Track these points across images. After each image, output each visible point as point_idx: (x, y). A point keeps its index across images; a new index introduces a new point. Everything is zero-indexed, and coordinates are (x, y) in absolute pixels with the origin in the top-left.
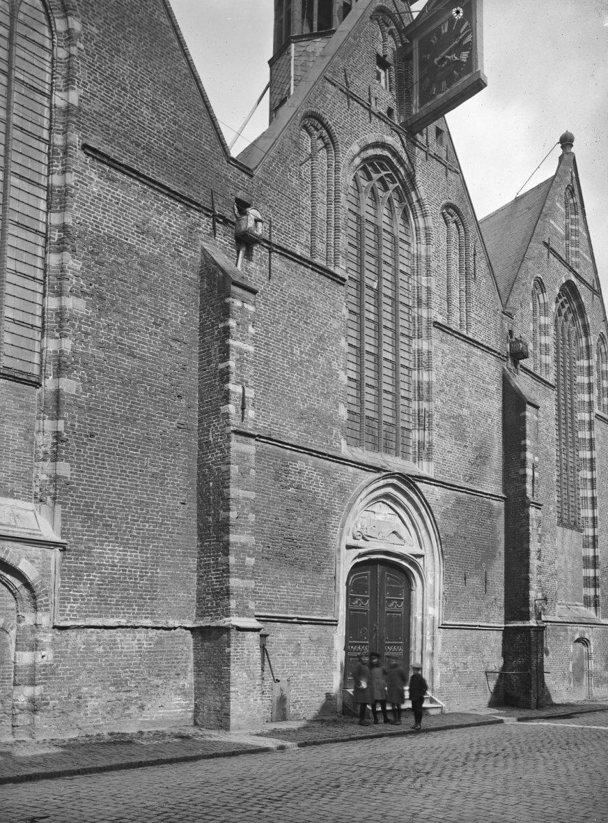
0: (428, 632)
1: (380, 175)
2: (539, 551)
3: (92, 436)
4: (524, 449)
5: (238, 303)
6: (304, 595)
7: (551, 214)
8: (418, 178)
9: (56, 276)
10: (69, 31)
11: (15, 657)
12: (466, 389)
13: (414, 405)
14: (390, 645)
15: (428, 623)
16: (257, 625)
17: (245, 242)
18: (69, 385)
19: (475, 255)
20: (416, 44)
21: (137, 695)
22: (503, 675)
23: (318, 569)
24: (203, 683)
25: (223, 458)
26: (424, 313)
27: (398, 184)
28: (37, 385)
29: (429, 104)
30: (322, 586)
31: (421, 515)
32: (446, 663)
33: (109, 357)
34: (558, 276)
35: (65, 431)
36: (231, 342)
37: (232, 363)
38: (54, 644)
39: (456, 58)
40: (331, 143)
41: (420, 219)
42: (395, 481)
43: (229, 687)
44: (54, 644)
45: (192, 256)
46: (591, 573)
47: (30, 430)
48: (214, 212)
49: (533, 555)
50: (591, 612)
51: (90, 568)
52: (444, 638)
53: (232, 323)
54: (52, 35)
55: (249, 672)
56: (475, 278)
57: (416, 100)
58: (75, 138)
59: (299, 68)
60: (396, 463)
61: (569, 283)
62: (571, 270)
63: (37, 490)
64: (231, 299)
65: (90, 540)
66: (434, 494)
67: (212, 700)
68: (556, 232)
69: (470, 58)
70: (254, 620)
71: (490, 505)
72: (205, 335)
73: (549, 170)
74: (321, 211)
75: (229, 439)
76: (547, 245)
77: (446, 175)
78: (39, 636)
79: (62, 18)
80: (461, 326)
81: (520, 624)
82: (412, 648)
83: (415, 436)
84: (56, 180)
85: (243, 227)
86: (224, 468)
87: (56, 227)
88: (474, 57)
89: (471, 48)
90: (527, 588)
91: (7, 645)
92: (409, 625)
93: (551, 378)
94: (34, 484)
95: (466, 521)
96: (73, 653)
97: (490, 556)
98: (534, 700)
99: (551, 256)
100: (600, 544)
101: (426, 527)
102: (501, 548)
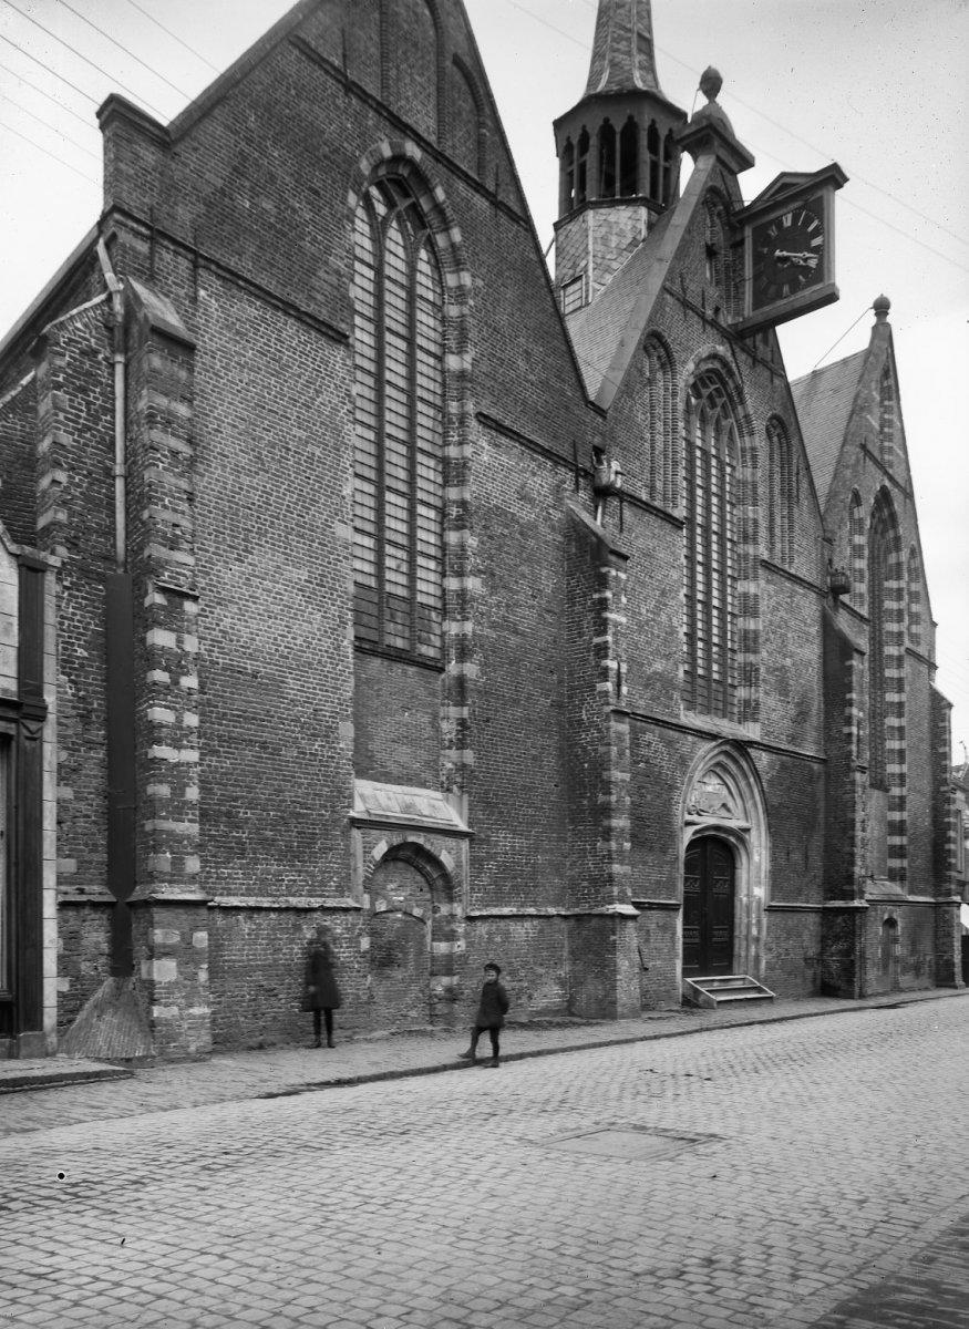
2: (863, 822)
3: (488, 721)
5: (613, 573)
6: (654, 878)
11: (431, 949)
12: (789, 635)
13: (740, 657)
14: (719, 929)
17: (602, 493)
18: (471, 669)
19: (798, 474)
20: (748, 232)
21: (526, 984)
23: (664, 850)
27: (725, 399)
31: (749, 785)
32: (770, 950)
34: (872, 482)
35: (470, 718)
36: (611, 616)
38: (467, 935)
42: (727, 748)
44: (467, 935)
46: (897, 840)
47: (435, 716)
51: (492, 857)
54: (443, 291)
55: (630, 960)
58: (470, 407)
60: (727, 727)
61: (883, 488)
65: (489, 829)
68: (872, 427)
69: (820, 265)
70: (631, 907)
71: (811, 769)
77: (772, 381)
78: (454, 926)
79: (453, 272)
84: (453, 452)
86: (602, 749)
87: (454, 502)
88: (825, 265)
89: (824, 253)
90: (853, 864)
92: (732, 907)
93: (864, 612)
94: (441, 773)
98: (857, 990)
100: (908, 806)
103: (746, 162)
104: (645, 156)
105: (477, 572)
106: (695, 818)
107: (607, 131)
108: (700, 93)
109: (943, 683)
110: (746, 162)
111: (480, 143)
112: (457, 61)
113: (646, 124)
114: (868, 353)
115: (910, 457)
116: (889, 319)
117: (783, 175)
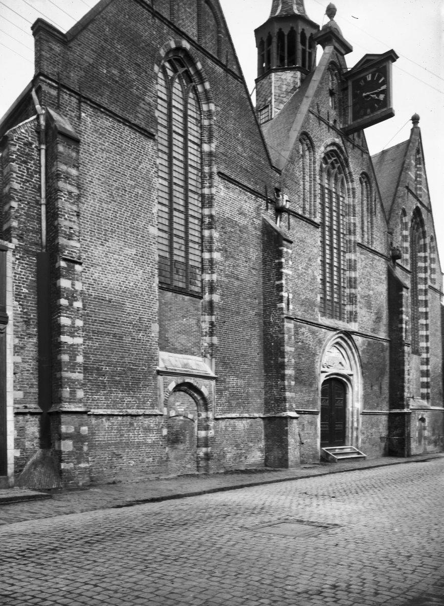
0: (355, 417)
1: (332, 160)
4: (402, 313)
6: (306, 399)
7: (408, 169)
8: (350, 160)
9: (208, 241)
10: (209, 111)
12: (372, 280)
13: (347, 291)
15: (355, 412)
16: (297, 415)
20: (350, 83)
22: (389, 438)
24: (270, 445)
25: (280, 331)
26: (352, 238)
28: (201, 298)
29: (359, 120)
30: (312, 394)
31: (352, 353)
32: (363, 433)
33: (230, 281)
36: (283, 270)
37: (283, 282)
38: (215, 427)
39: (376, 98)
40: (312, 147)
41: (350, 184)
43: (287, 447)
45: (258, 222)
47: (199, 321)
48: (266, 198)
49: (406, 373)
50: (425, 403)
52: (363, 420)
53: (283, 260)
56: (375, 215)
57: (350, 116)
58: (215, 169)
59: (277, 88)
60: (342, 325)
61: (417, 208)
62: (418, 200)
63: (203, 351)
64: (282, 248)
66: (359, 340)
67: (277, 453)
71: (383, 345)
72: (266, 265)
73: (407, 137)
74: (307, 185)
75: (283, 321)
76: (407, 187)
78: (209, 423)
79: (206, 104)
80: (368, 243)
81: (398, 411)
82: (347, 425)
83: (348, 308)
84: (206, 191)
85: (281, 205)
86: (280, 336)
87: (207, 216)
89: (387, 92)
91: (193, 428)
95: (372, 354)
96: (221, 431)
97: (382, 374)
98: (406, 453)
99: (409, 194)
100: (430, 363)
101: (354, 359)
102: (388, 369)
103: (349, 50)
104: (300, 47)
105: (219, 250)
107: (281, 34)
110: (349, 50)
113: (300, 31)
116: (419, 125)
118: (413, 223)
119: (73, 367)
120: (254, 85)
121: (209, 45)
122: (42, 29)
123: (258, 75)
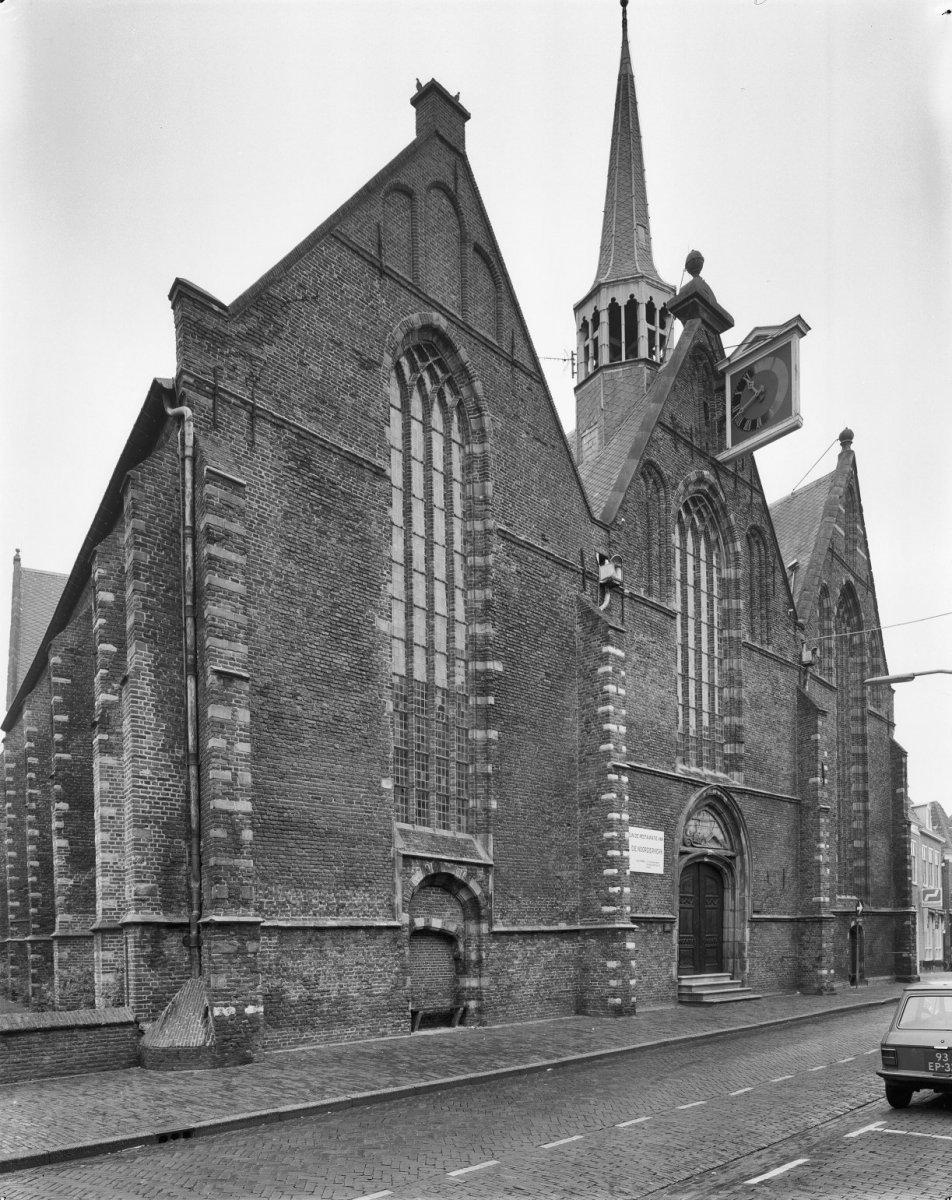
61: (848, 583)
62: (850, 570)
82: (726, 924)
103: (726, 322)
104: (643, 328)
106: (689, 849)
107: (614, 308)
108: (687, 273)
109: (899, 736)
110: (726, 322)
111: (498, 315)
112: (478, 249)
113: (646, 300)
114: (833, 477)
115: (871, 558)
116: (852, 447)
117: (757, 329)
118: (841, 610)
119: (231, 791)
120: (572, 399)
121: (480, 317)
122: (184, 294)
123: (418, 130)
